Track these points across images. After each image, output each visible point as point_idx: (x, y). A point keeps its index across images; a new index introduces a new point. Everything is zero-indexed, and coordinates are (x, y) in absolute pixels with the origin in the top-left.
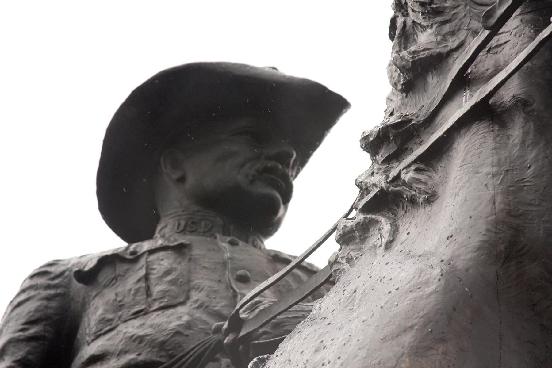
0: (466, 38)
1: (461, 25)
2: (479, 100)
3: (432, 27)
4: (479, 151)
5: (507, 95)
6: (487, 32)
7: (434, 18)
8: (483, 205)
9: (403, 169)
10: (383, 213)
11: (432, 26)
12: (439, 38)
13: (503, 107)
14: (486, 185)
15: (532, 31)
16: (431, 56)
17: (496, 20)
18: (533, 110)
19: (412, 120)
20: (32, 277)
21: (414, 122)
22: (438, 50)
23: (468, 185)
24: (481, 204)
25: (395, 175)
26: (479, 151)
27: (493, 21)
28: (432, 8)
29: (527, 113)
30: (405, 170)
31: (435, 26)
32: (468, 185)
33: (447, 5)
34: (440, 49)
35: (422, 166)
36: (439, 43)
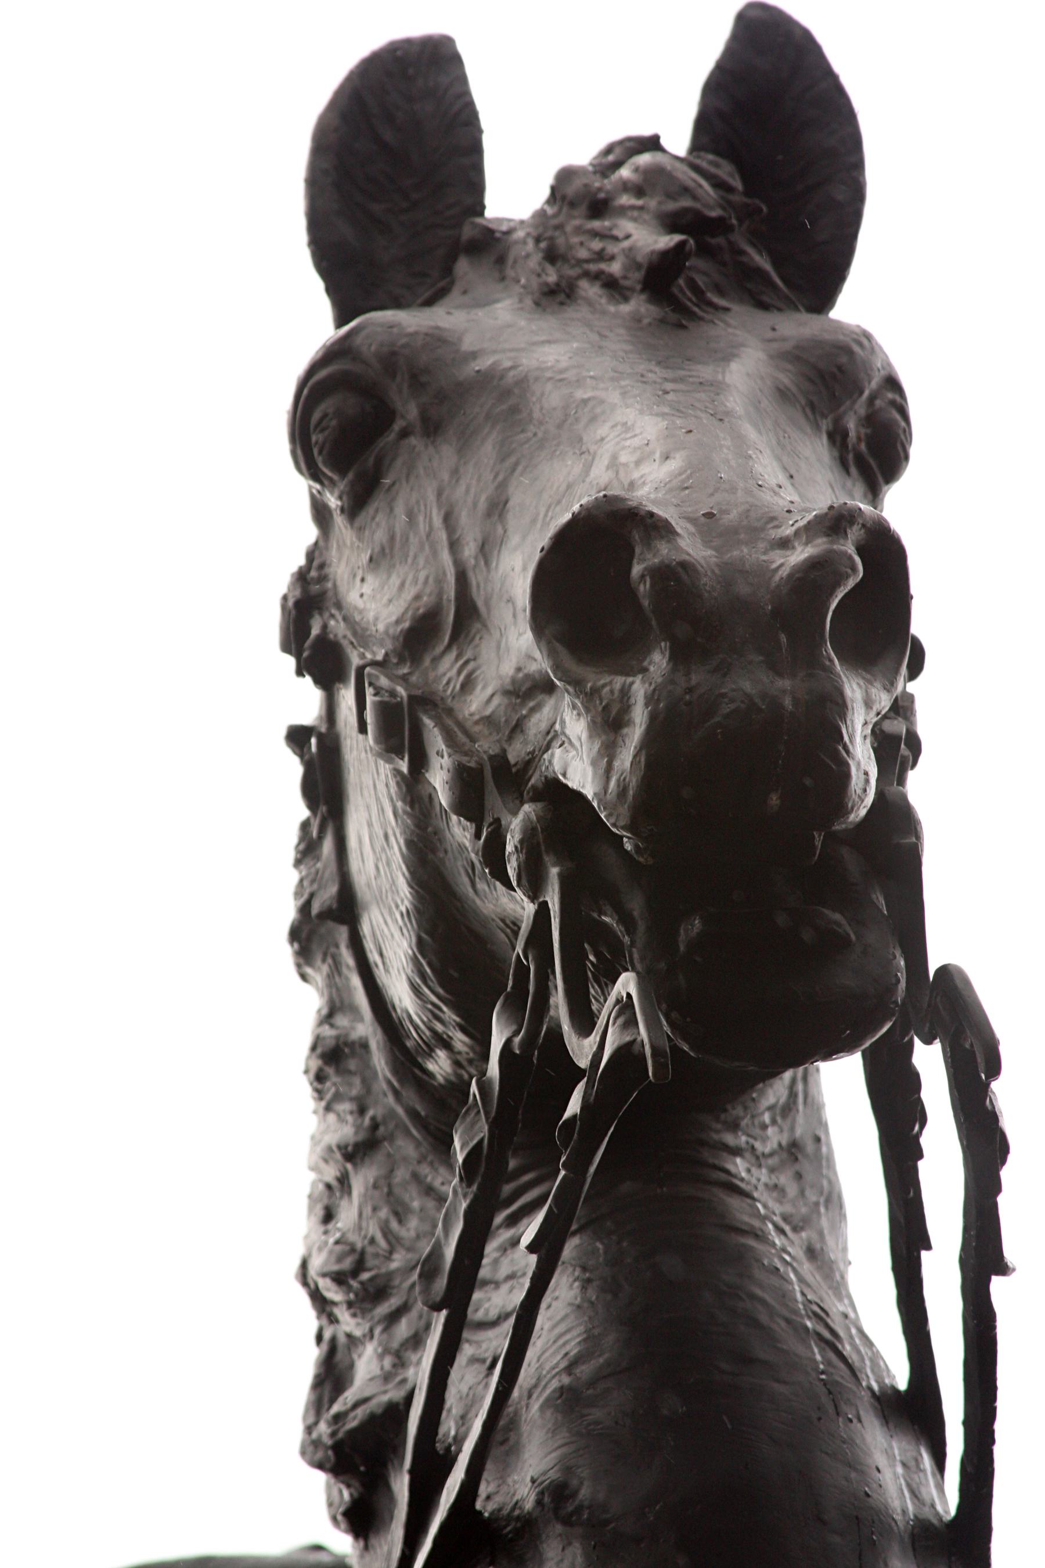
3: (372, 1337)
7: (371, 1310)
10: (850, 805)
12: (388, 1362)
13: (518, 1518)
15: (577, 1284)
16: (372, 1418)
18: (579, 1509)
22: (385, 1398)
27: (441, 1283)
28: (362, 1283)
29: (567, 1522)
31: (378, 1331)
33: (394, 1265)
36: (387, 1377)
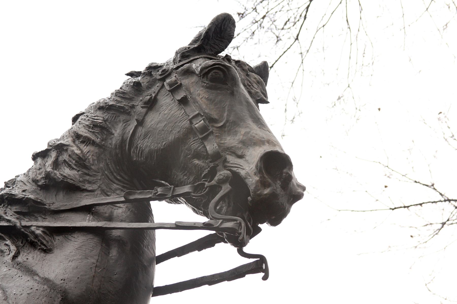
0: (97, 189)
1: (96, 182)
2: (104, 226)
4: (91, 249)
5: (116, 233)
6: (123, 199)
8: (87, 276)
9: (35, 226)
11: (78, 171)
14: (91, 268)
17: (133, 198)
19: (45, 205)
20: (198, 214)
21: (46, 207)
22: (79, 185)
23: (80, 261)
24: (85, 275)
25: (27, 225)
26: (91, 249)
30: (35, 227)
31: (80, 173)
32: (80, 261)
34: (80, 185)
35: (48, 232)
